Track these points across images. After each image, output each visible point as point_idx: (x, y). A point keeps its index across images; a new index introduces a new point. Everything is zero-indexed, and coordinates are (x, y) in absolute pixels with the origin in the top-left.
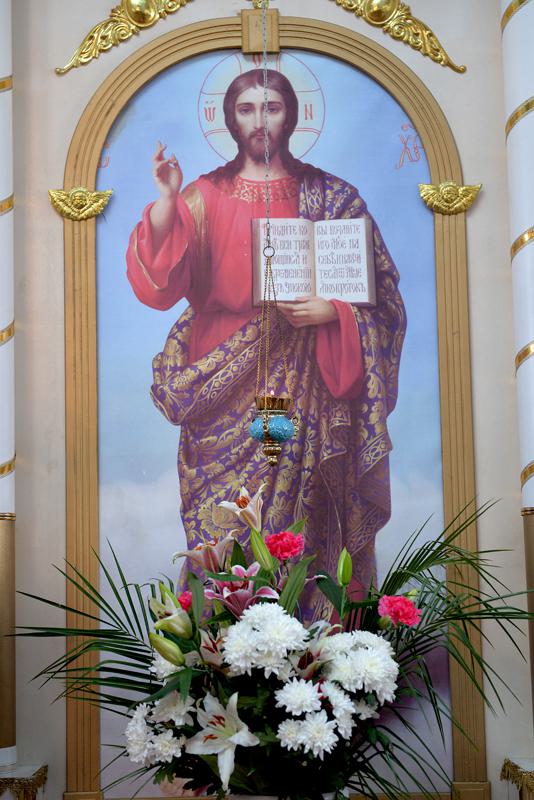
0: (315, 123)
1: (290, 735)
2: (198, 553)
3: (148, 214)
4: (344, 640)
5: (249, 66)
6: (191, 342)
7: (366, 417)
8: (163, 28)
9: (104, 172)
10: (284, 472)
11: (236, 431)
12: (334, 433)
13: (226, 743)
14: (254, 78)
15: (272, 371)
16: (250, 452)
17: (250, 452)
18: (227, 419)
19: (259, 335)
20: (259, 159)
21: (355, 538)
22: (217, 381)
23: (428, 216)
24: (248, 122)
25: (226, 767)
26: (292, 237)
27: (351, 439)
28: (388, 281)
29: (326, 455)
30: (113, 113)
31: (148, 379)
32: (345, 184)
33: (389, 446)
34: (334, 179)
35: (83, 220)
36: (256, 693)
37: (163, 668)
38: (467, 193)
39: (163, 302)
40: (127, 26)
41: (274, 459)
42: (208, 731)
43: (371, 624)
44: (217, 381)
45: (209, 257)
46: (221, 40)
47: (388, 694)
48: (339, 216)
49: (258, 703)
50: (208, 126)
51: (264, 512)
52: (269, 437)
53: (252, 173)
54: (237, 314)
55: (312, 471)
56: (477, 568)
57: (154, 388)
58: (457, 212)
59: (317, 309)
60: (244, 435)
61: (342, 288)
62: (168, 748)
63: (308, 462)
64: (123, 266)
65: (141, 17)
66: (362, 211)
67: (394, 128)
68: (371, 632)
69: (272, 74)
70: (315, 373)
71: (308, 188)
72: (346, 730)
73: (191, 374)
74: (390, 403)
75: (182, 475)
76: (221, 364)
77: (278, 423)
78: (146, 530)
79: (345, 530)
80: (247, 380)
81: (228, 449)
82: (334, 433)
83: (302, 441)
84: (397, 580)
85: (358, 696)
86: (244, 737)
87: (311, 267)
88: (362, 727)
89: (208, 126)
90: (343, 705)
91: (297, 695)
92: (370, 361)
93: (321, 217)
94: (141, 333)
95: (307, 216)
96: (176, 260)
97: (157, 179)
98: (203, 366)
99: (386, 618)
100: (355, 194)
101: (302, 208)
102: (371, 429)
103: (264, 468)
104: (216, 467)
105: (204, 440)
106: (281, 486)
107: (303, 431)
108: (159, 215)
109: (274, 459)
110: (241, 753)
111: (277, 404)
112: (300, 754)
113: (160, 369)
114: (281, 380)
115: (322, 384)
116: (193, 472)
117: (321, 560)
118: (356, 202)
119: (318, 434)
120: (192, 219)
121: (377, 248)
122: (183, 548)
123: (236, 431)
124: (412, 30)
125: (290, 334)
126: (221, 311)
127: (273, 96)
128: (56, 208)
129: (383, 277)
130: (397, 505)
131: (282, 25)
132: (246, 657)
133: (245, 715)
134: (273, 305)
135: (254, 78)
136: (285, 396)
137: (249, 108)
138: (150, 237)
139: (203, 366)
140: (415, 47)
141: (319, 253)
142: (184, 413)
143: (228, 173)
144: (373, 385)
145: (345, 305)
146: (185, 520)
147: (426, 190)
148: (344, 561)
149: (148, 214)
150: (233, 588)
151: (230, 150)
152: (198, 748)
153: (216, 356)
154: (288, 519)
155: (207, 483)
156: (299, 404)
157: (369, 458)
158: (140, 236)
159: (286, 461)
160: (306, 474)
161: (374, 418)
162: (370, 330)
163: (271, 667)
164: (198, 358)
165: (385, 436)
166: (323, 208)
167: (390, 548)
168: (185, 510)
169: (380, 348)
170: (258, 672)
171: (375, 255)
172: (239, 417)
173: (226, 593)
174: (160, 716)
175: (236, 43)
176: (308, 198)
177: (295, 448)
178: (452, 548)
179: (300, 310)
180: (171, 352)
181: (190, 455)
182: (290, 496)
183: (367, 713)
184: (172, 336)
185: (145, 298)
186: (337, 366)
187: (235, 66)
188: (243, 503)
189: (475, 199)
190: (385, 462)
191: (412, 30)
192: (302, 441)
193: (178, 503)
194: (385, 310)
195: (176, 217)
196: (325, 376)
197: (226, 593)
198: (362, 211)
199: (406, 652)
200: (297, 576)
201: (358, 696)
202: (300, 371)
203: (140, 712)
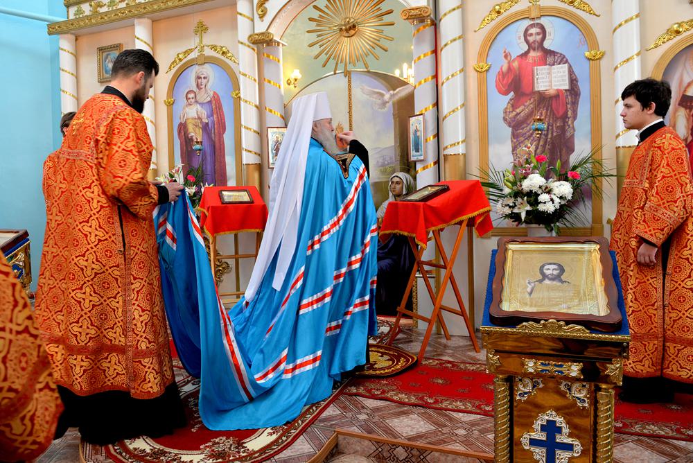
0: (552, 37)
1: (541, 207)
2: (517, 162)
3: (501, 69)
4: (558, 183)
5: (531, 22)
6: (514, 104)
7: (567, 122)
8: (505, 15)
9: (488, 58)
10: (542, 139)
11: (528, 128)
12: (557, 127)
13: (523, 209)
14: (532, 26)
15: (538, 111)
16: (532, 134)
17: (532, 134)
18: (525, 125)
19: (535, 100)
20: (534, 50)
21: (564, 157)
22: (522, 114)
23: (588, 61)
24: (531, 39)
25: (523, 216)
26: (544, 71)
27: (563, 129)
28: (575, 82)
29: (555, 134)
30: (491, 41)
31: (502, 115)
32: (561, 54)
33: (574, 131)
34: (558, 53)
35: (482, 73)
36: (532, 197)
37: (507, 191)
38: (600, 53)
39: (506, 93)
40: (494, 15)
41: (538, 136)
42: (519, 206)
43: (566, 180)
44: (522, 114)
45: (520, 79)
46: (523, 16)
47: (569, 197)
48: (559, 64)
49: (532, 199)
50: (519, 41)
51: (536, 151)
52: (537, 130)
53: (532, 54)
54: (528, 95)
55: (551, 138)
56: (601, 165)
57: (504, 118)
58: (597, 59)
59: (552, 92)
60: (530, 130)
61: (561, 85)
62: (507, 211)
63: (550, 136)
64: (494, 84)
65: (499, 12)
66: (567, 62)
67: (577, 35)
68: (603, 271)
69: (538, 24)
70: (552, 110)
71: (549, 57)
72: (558, 207)
73: (514, 113)
74: (575, 118)
75: (512, 141)
76: (523, 110)
77: (539, 125)
78: (502, 158)
79: (561, 155)
80: (531, 114)
81: (525, 134)
82: (557, 127)
83: (548, 130)
84: (575, 168)
85: (561, 198)
86: (529, 208)
87: (550, 79)
88: (562, 206)
89: (519, 41)
90: (557, 200)
91: (544, 197)
92: (569, 106)
93: (554, 65)
94: (500, 103)
95: (549, 65)
96: (510, 81)
97: (504, 59)
98: (518, 111)
99: (570, 178)
100: (564, 57)
101: (548, 62)
102: (569, 126)
103: (536, 138)
104: (522, 139)
105: (518, 132)
106: (541, 143)
107: (548, 128)
108: (505, 69)
109: (538, 136)
110: (528, 212)
111: (540, 120)
112: (543, 213)
113: (505, 112)
114: (541, 113)
115: (554, 113)
116: (515, 140)
117: (552, 163)
118: (565, 59)
119: (552, 128)
120: (514, 68)
121: (571, 72)
122: (512, 160)
123: (528, 128)
124: (582, 5)
125: (544, 100)
126: (524, 95)
127: (538, 30)
128: (475, 69)
129: (573, 81)
130: (576, 147)
131: (541, 9)
132: (528, 187)
133: (528, 202)
134: (539, 92)
135: (532, 26)
136: (542, 118)
137: (531, 35)
138: (502, 75)
139: (518, 111)
140: (583, 10)
141: (553, 75)
142: (512, 125)
143: (526, 54)
144: (570, 113)
145: (561, 90)
146: (513, 154)
147: (587, 54)
148: (558, 163)
149: (501, 69)
150: (526, 170)
151: (526, 48)
152: (516, 211)
153: (522, 107)
154: (543, 152)
155: (520, 143)
156: (547, 120)
157: (568, 134)
158: (499, 75)
159: (543, 136)
160: (549, 140)
161: (570, 123)
162: (569, 97)
163: (535, 190)
164: (516, 109)
165: (573, 128)
166: (554, 62)
167: (573, 159)
168: (513, 151)
169: (572, 102)
170: (531, 191)
171: (571, 75)
172: (529, 124)
173: (524, 171)
174: (506, 203)
175: (528, 16)
176: (550, 59)
177: (545, 132)
178: (595, 159)
179: (547, 93)
180: (508, 107)
181: (514, 136)
182: (544, 146)
183: (563, 203)
184: (509, 103)
185: (500, 92)
186: (559, 108)
187: (527, 23)
188: (529, 148)
189: (603, 55)
190: (573, 135)
191: (582, 5)
192: (548, 130)
193: (511, 149)
194: (574, 91)
195: (510, 69)
196: (555, 111)
197: (524, 171)
198: (567, 62)
199: (576, 187)
200: (545, 166)
201: (561, 198)
202: (547, 110)
203: (500, 203)
